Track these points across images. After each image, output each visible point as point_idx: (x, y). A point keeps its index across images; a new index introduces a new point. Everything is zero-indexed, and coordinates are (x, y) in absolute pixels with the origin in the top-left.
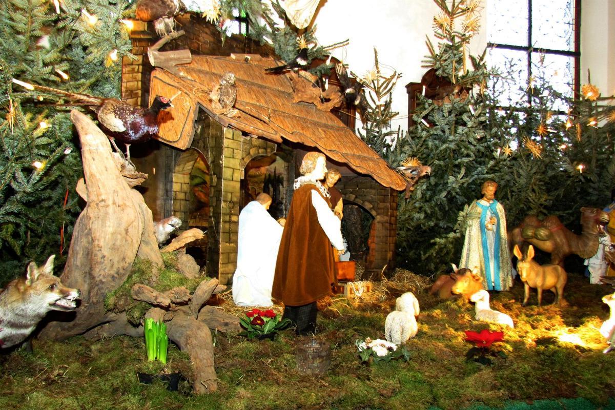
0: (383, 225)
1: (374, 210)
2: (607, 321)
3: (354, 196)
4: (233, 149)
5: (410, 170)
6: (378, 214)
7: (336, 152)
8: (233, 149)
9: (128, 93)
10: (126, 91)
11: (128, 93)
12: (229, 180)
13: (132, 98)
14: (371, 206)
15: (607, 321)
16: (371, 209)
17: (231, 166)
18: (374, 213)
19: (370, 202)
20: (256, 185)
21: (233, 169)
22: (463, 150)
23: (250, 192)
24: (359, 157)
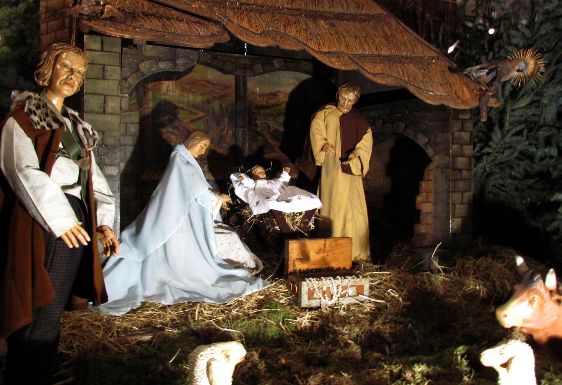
0: (442, 172)
1: (431, 146)
2: (500, 377)
3: (403, 125)
4: (104, 66)
5: (486, 71)
6: (436, 153)
7: (338, 55)
8: (104, 66)
9: (48, 14)
10: (47, 12)
11: (48, 14)
12: (98, 113)
13: (55, 19)
14: (427, 140)
15: (500, 377)
16: (426, 144)
17: (101, 91)
18: (430, 152)
19: (425, 133)
20: (271, 119)
21: (105, 96)
22: (167, 36)
23: (258, 130)
24: (388, 59)
